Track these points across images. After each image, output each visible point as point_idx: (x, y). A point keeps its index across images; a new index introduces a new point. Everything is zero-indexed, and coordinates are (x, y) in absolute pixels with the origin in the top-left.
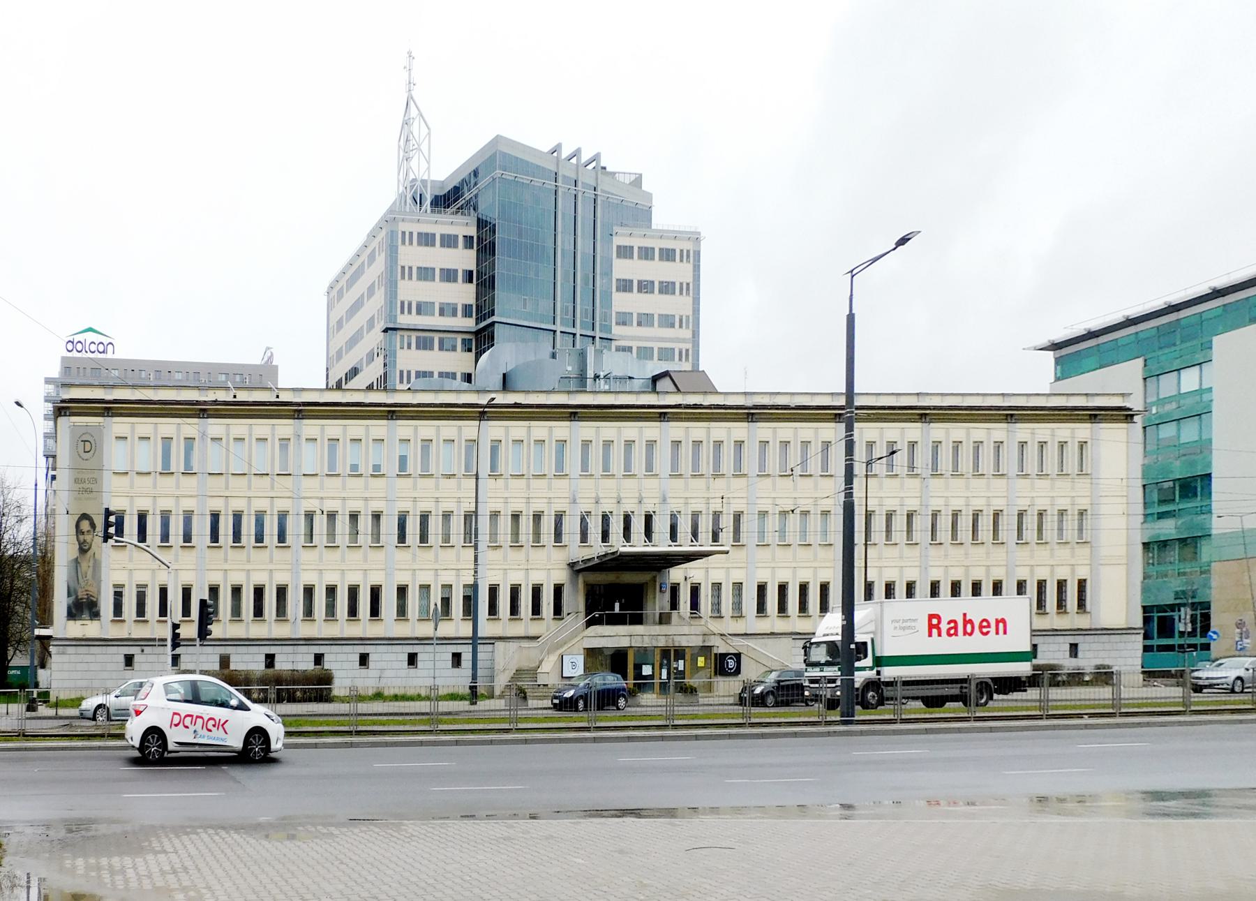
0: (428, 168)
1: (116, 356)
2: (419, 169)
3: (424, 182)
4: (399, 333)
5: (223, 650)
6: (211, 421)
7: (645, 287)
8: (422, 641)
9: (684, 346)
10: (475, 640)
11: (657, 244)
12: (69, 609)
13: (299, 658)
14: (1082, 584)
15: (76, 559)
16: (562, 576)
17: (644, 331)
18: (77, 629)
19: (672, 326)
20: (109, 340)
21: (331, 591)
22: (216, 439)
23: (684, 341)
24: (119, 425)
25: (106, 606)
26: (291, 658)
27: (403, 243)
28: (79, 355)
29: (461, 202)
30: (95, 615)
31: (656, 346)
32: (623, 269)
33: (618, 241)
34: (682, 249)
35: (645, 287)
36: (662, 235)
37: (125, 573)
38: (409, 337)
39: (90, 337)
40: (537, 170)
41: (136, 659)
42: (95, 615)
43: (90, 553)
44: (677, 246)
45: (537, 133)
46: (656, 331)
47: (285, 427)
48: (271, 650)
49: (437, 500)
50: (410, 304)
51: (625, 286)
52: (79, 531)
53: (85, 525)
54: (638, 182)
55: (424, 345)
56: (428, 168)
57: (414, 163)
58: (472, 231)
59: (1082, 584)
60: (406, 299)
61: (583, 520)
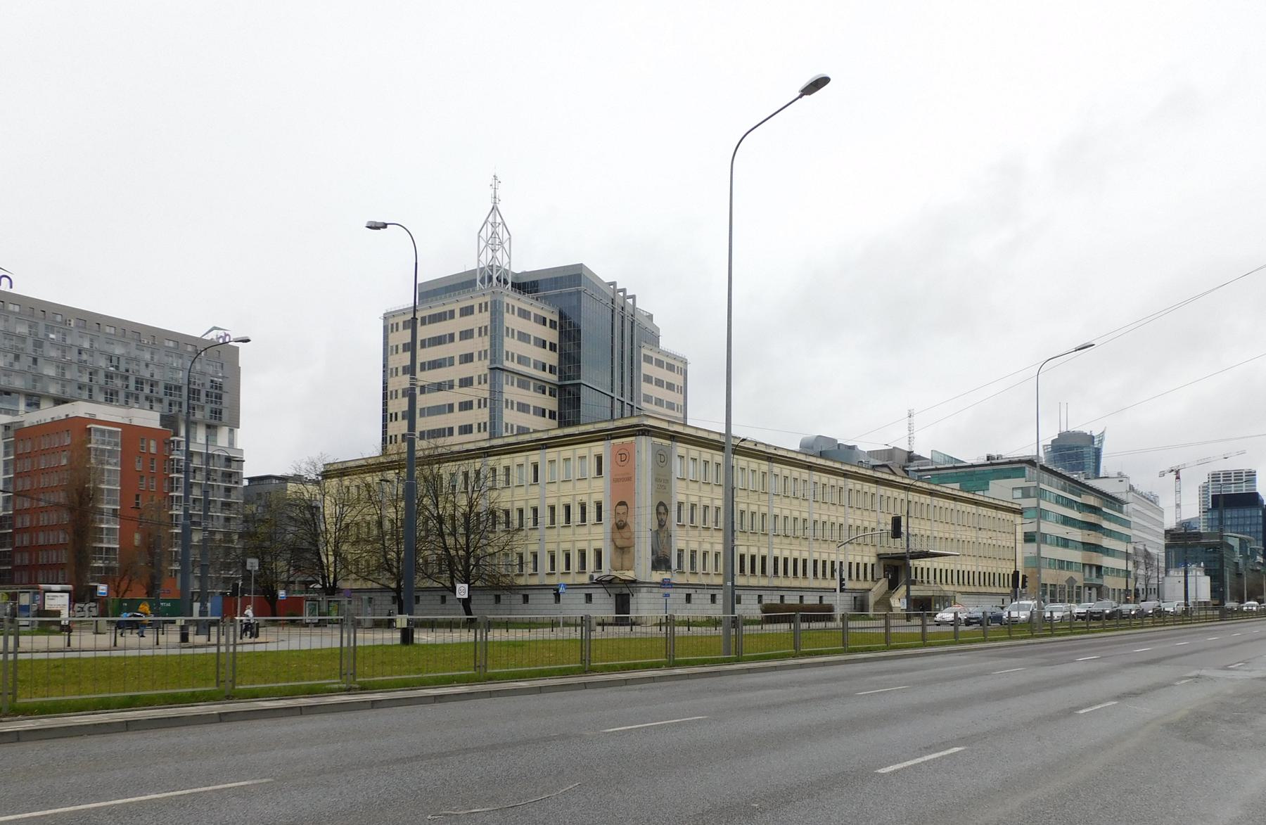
1: (12, 291)
2: (502, 259)
7: (659, 383)
11: (655, 356)
15: (657, 532)
16: (874, 560)
18: (657, 577)
21: (583, 554)
22: (754, 471)
24: (680, 449)
30: (668, 568)
33: (644, 351)
34: (678, 366)
35: (659, 383)
36: (668, 355)
42: (668, 568)
44: (677, 364)
45: (604, 270)
47: (764, 466)
48: (690, 591)
49: (712, 499)
51: (648, 379)
52: (658, 513)
53: (662, 509)
54: (650, 317)
57: (499, 254)
58: (556, 318)
60: (510, 350)
61: (536, 479)
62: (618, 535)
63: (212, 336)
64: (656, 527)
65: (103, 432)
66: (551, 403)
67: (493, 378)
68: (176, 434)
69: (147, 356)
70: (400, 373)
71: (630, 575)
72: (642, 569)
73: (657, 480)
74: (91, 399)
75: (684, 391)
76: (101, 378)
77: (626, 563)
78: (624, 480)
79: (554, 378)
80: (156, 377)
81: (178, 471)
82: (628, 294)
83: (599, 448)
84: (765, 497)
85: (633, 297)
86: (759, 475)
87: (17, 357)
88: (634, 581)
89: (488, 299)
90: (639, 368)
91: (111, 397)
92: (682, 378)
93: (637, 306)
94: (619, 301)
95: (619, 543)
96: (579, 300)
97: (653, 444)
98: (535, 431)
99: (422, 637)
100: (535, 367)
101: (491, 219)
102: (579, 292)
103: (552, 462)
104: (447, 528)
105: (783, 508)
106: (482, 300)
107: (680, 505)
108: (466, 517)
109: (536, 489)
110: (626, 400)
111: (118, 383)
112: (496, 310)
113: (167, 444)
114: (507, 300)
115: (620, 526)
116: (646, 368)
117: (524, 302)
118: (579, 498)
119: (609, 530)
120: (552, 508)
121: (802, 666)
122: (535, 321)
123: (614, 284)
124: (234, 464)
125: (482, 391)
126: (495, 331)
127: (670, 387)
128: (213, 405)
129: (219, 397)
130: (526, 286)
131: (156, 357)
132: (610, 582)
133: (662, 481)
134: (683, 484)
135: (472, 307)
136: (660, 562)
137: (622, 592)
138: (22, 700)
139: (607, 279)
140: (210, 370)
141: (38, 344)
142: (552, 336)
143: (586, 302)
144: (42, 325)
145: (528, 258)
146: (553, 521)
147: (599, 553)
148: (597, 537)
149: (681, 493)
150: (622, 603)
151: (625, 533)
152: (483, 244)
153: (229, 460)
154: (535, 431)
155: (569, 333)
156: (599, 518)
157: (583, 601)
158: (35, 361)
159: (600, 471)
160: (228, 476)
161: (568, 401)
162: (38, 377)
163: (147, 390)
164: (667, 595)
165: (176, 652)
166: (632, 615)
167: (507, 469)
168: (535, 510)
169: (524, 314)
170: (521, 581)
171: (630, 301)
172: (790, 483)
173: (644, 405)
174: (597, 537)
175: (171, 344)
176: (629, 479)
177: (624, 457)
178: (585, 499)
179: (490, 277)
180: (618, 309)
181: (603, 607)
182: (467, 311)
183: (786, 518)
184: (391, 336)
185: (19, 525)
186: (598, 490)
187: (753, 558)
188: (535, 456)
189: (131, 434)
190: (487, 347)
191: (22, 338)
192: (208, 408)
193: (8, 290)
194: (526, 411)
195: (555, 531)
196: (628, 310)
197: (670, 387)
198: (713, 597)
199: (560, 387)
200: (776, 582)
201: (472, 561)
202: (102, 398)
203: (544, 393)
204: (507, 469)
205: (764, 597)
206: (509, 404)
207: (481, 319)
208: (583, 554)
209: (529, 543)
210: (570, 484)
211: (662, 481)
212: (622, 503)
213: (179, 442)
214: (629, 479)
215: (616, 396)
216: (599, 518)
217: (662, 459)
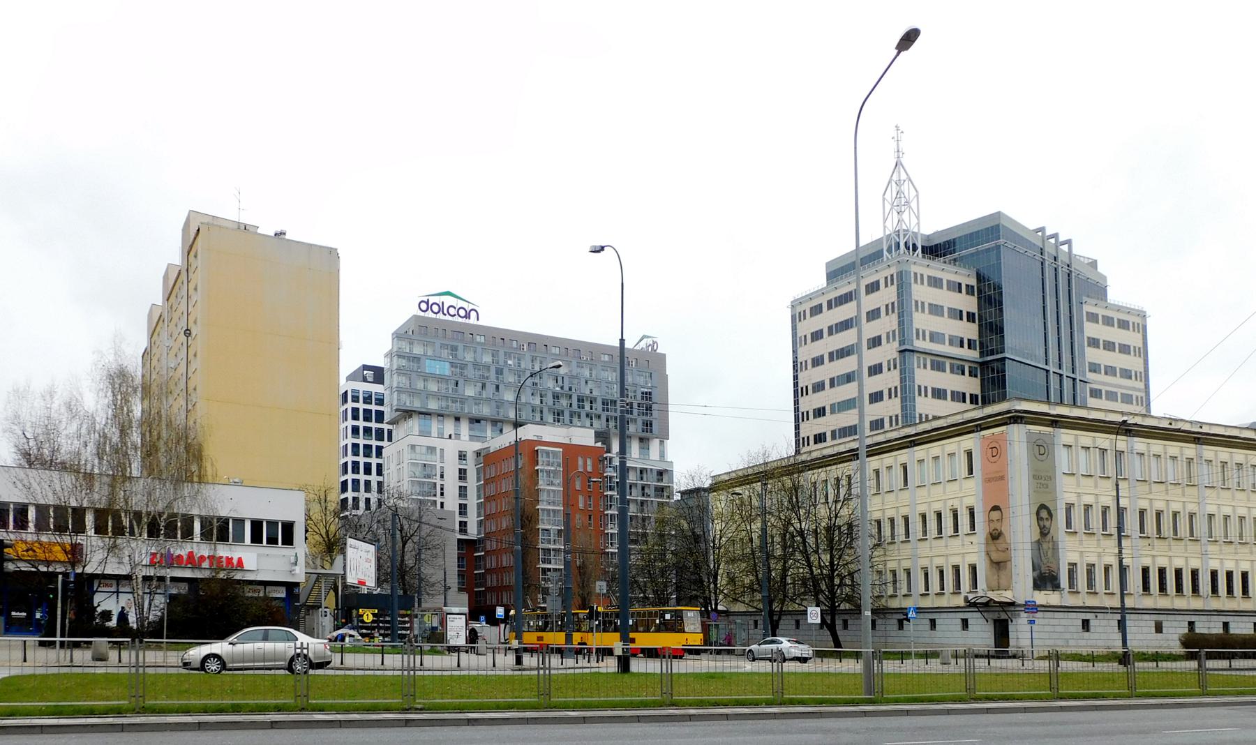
0: (885, 221)
1: (480, 323)
2: (909, 222)
3: (915, 234)
4: (916, 355)
5: (1225, 619)
6: (1136, 439)
7: (1109, 346)
8: (1196, 612)
9: (1140, 394)
10: (1123, 610)
11: (1101, 312)
12: (1035, 580)
13: (1212, 625)
14: (1245, 576)
15: (1038, 542)
17: (1109, 379)
18: (1041, 598)
19: (1130, 378)
20: (471, 307)
21: (957, 570)
22: (1174, 458)
23: (1139, 390)
24: (1066, 436)
25: (1064, 581)
26: (1207, 624)
27: (916, 281)
28: (450, 318)
29: (955, 255)
30: (1056, 587)
31: (1119, 391)
32: (1091, 330)
33: (1087, 308)
34: (1134, 322)
35: (1109, 346)
36: (1119, 309)
37: (1077, 554)
38: (925, 360)
39: (448, 301)
40: (1031, 245)
41: (1092, 623)
42: (1056, 587)
43: (1049, 536)
45: (1028, 213)
46: (1118, 380)
47: (1190, 450)
48: (1193, 618)
50: (924, 332)
51: (1094, 343)
52: (1039, 518)
53: (1044, 514)
54: (1094, 264)
55: (937, 367)
56: (885, 221)
57: (905, 216)
58: (973, 282)
59: (1245, 576)
60: (921, 327)
62: (993, 548)
63: (643, 345)
64: (1037, 536)
65: (547, 453)
66: (971, 385)
67: (903, 363)
68: (609, 451)
69: (587, 373)
70: (809, 366)
71: (1007, 596)
72: (1021, 588)
73: (1034, 477)
74: (542, 422)
75: (1143, 352)
76: (549, 400)
77: (1003, 582)
78: (997, 479)
79: (974, 355)
80: (595, 393)
81: (611, 489)
82: (1061, 239)
83: (969, 442)
84: (1194, 491)
85: (1068, 242)
86: (1182, 466)
87: (484, 386)
88: (1013, 604)
89: (893, 270)
90: (1082, 332)
91: (558, 416)
92: (1140, 336)
93: (1075, 251)
94: (1049, 250)
95: (995, 557)
96: (999, 258)
97: (1029, 433)
98: (935, 418)
99: (637, 665)
100: (951, 343)
101: (895, 177)
102: (998, 247)
103: (921, 461)
104: (811, 540)
105: (1219, 504)
106: (887, 273)
107: (1069, 507)
108: (829, 529)
109: (906, 494)
110: (1066, 372)
111: (564, 402)
112: (902, 282)
113: (600, 458)
114: (914, 269)
115: (995, 536)
116: (1091, 330)
117: (936, 268)
118: (950, 503)
119: (983, 540)
120: (924, 517)
121: (1062, 709)
122: (949, 289)
123: (1042, 229)
124: (665, 478)
125: (889, 379)
126: (902, 308)
127: (1125, 349)
128: (645, 418)
129: (649, 408)
130: (936, 250)
131: (594, 373)
132: (986, 604)
133: (1043, 479)
134: (1072, 480)
135: (878, 282)
136: (1046, 580)
137: (1001, 617)
138: (150, 702)
139: (1032, 226)
140: (641, 380)
141: (499, 372)
142: (969, 304)
143: (1007, 259)
144: (501, 354)
145: (934, 221)
146: (925, 532)
147: (973, 569)
148: (969, 550)
149: (1067, 491)
150: (1002, 632)
151: (1000, 544)
152: (888, 207)
153: (660, 473)
154: (935, 418)
155: (989, 297)
156: (973, 527)
157: (959, 627)
158: (497, 387)
159: (971, 471)
160: (660, 490)
161: (992, 376)
162: (500, 404)
163: (587, 407)
164: (1032, 622)
165: (509, 673)
166: (1011, 650)
167: (877, 472)
168: (906, 519)
169: (935, 282)
170: (894, 604)
171: (1065, 248)
172: (1231, 472)
173: (1090, 376)
174: (969, 550)
175: (606, 358)
176: (1002, 478)
177: (995, 451)
178: (957, 504)
179: (904, 244)
180: (1049, 261)
181: (981, 634)
182: (873, 288)
183: (1226, 517)
184: (799, 325)
185: (488, 548)
186: (969, 493)
187: (1229, 575)
188: (903, 456)
189: (571, 452)
190: (895, 327)
191: (488, 368)
192: (640, 420)
193: (476, 322)
194: (943, 393)
195: (926, 544)
196: (1063, 258)
197: (1125, 349)
198: (756, 622)
199: (981, 364)
200: (1214, 604)
201: (837, 581)
202: (550, 418)
203: (963, 374)
204: (877, 472)
205: (1231, 625)
206: (923, 391)
207: (888, 295)
208: (957, 570)
209: (897, 558)
210: (940, 487)
211: (1043, 479)
212: (996, 508)
213: (611, 459)
214: (1002, 478)
215: (1052, 368)
216: (973, 527)
217: (1041, 450)
